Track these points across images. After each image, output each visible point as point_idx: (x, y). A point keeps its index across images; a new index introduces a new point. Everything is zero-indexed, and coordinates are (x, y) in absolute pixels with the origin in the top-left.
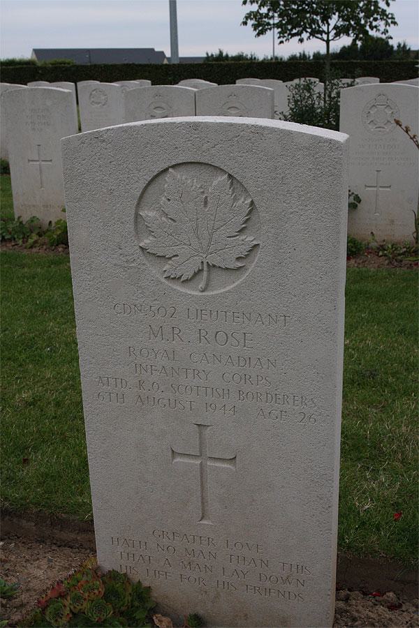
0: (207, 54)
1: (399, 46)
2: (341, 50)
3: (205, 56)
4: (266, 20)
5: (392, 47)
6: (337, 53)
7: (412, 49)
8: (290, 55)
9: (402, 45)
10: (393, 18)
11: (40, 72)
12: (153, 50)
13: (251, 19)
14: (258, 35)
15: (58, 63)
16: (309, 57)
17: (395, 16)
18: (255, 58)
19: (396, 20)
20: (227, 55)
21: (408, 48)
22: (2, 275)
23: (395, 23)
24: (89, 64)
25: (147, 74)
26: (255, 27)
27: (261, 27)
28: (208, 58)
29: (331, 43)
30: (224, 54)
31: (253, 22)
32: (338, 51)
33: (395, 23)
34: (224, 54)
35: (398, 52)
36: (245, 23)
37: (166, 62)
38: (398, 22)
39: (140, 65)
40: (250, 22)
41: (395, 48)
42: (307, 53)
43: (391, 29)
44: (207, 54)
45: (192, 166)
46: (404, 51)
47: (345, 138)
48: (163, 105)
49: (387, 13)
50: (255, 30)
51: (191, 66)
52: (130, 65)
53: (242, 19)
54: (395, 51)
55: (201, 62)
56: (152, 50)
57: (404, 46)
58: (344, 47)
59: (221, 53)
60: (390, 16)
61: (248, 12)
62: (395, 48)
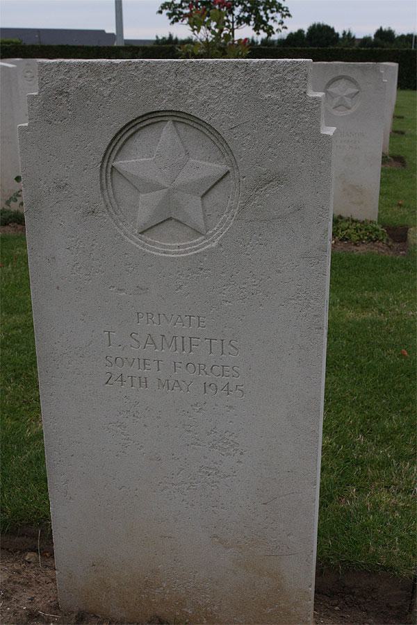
0: (157, 37)
1: (344, 34)
2: (288, 37)
3: (155, 39)
4: (180, 9)
5: (338, 35)
6: (284, 40)
8: (365, 35)
9: (347, 34)
10: (287, 11)
12: (103, 31)
13: (166, 9)
14: (173, 23)
15: (6, 43)
16: (257, 42)
17: (289, 10)
19: (290, 13)
20: (354, 37)
21: (352, 36)
22: (68, 624)
23: (289, 15)
24: (38, 44)
26: (170, 16)
27: (175, 16)
28: (157, 41)
29: (235, 31)
30: (174, 38)
31: (168, 11)
32: (285, 38)
33: (289, 15)
34: (174, 38)
36: (160, 12)
38: (292, 14)
39: (74, 47)
40: (165, 12)
41: (341, 36)
43: (287, 20)
44: (157, 37)
46: (349, 39)
48: (31, 70)
49: (283, 6)
50: (170, 18)
52: (64, 46)
53: (158, 9)
54: (341, 39)
55: (152, 45)
56: (103, 31)
57: (349, 34)
59: (171, 36)
60: (285, 9)
61: (164, 2)
62: (341, 36)
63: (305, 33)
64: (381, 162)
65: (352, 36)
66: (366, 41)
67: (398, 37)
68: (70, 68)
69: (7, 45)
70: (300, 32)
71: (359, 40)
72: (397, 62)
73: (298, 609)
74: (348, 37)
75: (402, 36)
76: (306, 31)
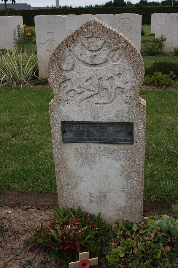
0: (52, 6)
1: (128, 2)
3: (51, 6)
5: (125, 3)
6: (83, 8)
7: (133, 3)
11: (65, 11)
12: (27, 4)
16: (93, 7)
18: (72, 7)
21: (131, 3)
25: (114, 12)
32: (105, 4)
35: (127, 4)
37: (32, 9)
41: (126, 3)
42: (92, 5)
44: (52, 6)
45: (78, 143)
47: (143, 104)
51: (37, 10)
57: (130, 2)
58: (107, 3)
59: (48, 6)
62: (126, 3)
63: (113, 2)
64: (141, 24)
65: (131, 3)
66: (137, 5)
67: (149, 3)
68: (44, 16)
69: (13, 10)
70: (111, 2)
71: (134, 4)
72: (170, 72)
73: (99, 158)
74: (129, 3)
75: (150, 3)
76: (113, 2)
